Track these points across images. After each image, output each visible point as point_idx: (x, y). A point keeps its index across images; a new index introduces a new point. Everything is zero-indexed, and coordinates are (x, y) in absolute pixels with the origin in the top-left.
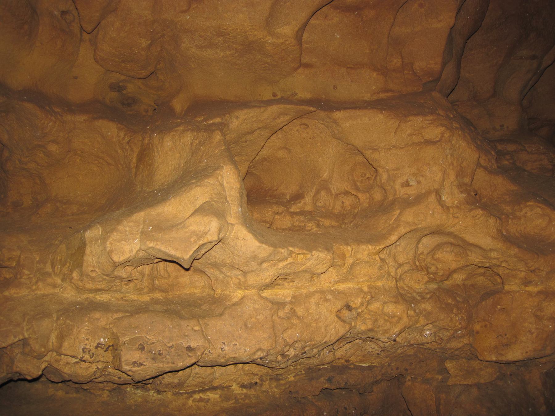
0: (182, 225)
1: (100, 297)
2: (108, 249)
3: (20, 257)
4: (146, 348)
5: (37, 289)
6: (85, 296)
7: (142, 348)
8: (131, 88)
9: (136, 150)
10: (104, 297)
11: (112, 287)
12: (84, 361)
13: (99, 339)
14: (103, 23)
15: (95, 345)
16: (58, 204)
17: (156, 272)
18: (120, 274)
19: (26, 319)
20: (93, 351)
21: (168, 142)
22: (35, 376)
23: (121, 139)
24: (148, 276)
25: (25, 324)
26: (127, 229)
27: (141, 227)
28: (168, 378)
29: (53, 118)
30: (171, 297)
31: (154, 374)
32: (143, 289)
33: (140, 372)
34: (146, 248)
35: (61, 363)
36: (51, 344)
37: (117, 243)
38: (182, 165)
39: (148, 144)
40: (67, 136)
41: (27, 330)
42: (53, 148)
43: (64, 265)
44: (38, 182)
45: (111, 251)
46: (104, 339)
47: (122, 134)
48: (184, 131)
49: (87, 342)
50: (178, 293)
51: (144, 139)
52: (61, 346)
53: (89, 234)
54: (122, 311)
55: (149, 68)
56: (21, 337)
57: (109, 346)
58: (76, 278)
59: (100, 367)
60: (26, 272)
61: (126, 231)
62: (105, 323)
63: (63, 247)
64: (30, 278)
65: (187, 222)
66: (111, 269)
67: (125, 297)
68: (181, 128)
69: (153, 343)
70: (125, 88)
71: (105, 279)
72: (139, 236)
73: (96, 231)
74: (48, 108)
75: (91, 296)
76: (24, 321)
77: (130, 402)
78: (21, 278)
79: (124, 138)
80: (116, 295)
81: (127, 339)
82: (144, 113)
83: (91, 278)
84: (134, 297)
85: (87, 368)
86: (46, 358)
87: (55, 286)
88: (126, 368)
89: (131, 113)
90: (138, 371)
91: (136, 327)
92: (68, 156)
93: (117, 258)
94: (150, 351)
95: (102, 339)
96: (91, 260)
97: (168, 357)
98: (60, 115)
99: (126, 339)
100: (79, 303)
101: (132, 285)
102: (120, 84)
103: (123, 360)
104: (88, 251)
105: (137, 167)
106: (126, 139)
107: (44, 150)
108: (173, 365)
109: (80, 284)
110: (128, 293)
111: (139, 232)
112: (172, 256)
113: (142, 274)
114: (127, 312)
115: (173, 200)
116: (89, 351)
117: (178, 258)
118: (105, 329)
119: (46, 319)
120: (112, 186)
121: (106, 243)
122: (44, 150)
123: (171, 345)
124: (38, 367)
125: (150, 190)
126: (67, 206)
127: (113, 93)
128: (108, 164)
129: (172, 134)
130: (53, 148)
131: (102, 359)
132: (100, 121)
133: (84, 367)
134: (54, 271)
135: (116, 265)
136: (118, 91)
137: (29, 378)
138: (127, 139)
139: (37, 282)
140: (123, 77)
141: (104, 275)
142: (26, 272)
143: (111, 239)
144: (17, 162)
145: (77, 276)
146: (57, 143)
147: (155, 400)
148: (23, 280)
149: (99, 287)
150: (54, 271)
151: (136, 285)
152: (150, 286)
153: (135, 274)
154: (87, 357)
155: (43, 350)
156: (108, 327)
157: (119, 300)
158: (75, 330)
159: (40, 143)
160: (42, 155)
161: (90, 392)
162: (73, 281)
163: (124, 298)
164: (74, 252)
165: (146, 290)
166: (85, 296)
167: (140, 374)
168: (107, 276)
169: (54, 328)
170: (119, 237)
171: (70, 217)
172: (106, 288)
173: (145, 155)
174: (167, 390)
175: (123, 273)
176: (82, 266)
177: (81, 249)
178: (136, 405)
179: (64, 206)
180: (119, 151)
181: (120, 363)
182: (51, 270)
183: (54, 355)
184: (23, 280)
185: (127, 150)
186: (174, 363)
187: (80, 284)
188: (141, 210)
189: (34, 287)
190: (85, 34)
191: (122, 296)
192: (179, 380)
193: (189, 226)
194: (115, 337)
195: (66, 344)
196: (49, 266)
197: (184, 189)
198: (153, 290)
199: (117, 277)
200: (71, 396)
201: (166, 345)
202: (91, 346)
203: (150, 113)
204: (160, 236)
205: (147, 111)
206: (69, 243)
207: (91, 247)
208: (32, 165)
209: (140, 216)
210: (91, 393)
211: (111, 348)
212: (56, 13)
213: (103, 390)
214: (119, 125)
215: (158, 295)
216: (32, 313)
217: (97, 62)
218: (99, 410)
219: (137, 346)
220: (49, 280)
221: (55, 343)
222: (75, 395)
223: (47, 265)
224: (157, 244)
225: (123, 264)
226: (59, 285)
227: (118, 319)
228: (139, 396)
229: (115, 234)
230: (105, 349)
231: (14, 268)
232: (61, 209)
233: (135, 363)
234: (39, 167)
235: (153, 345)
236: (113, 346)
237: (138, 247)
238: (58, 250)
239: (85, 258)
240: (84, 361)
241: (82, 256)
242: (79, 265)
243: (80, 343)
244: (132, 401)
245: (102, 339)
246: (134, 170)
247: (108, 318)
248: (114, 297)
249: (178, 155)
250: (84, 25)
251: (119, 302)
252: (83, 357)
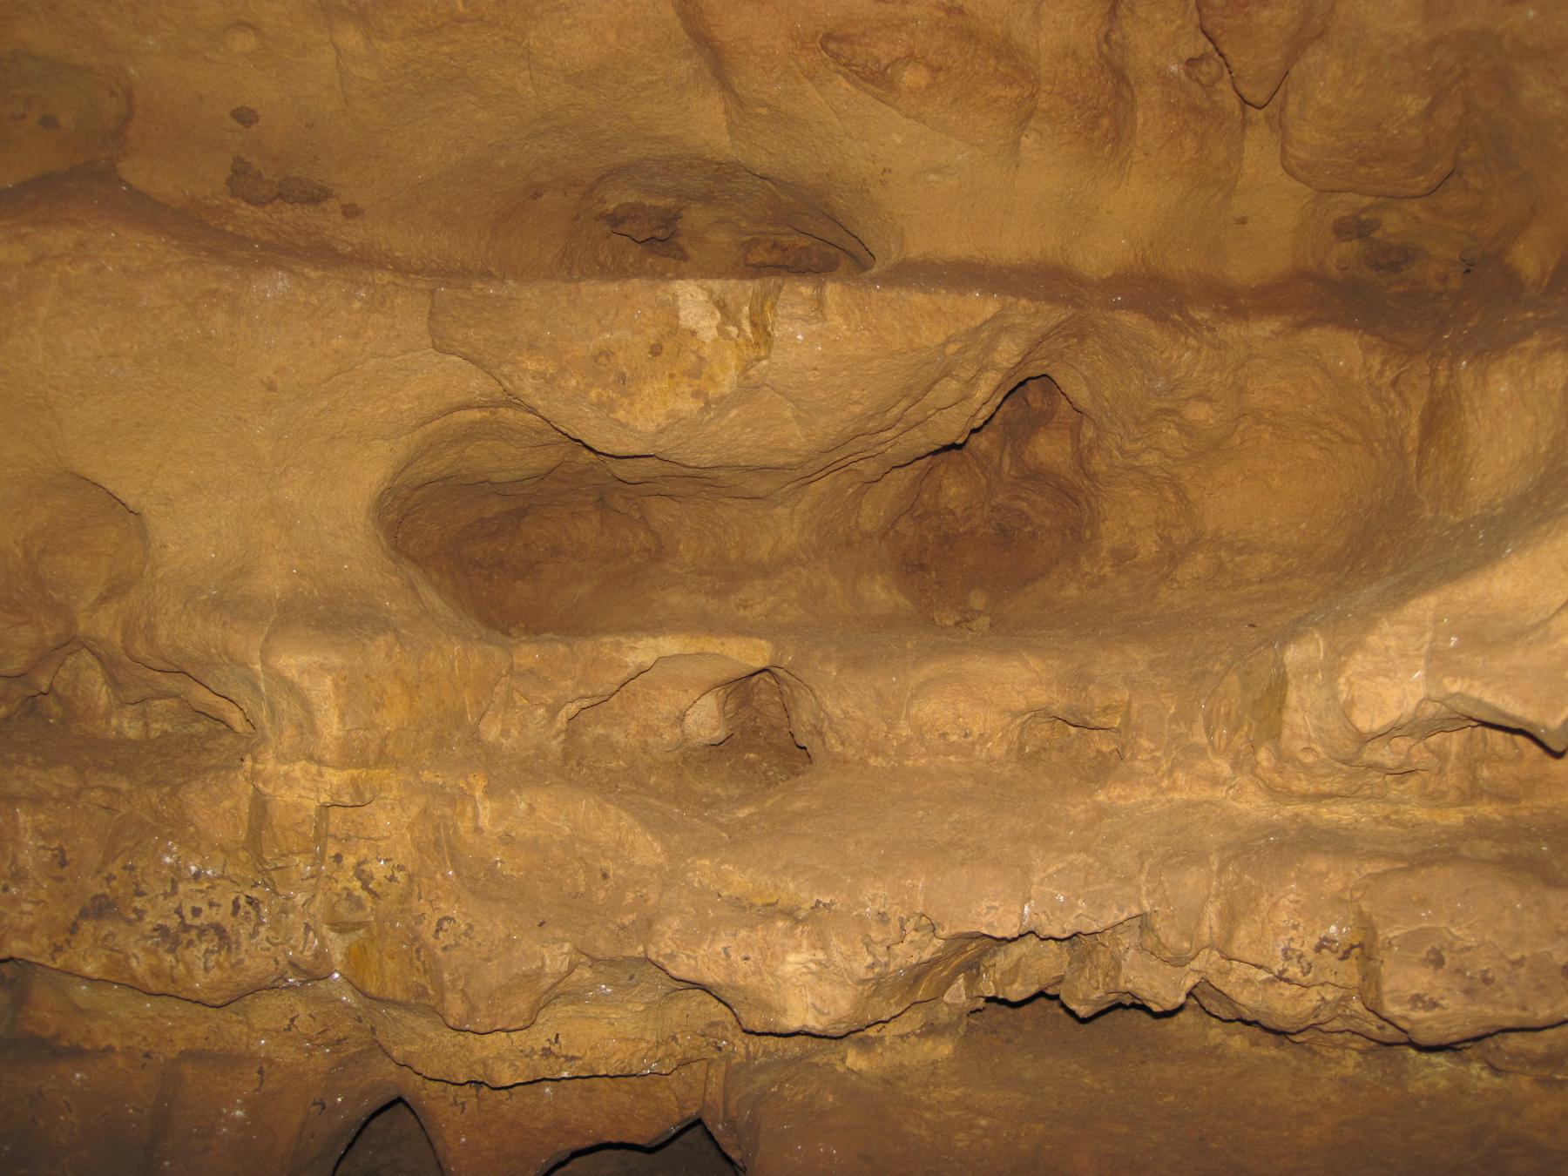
0: (1540, 632)
1: (1331, 812)
2: (1343, 697)
3: (1129, 703)
4: (1447, 960)
5: (1173, 787)
6: (1289, 810)
7: (1438, 962)
8: (1392, 224)
9: (1418, 403)
10: (1342, 814)
11: (1360, 788)
12: (1287, 980)
13: (1326, 926)
14: (1294, 72)
15: (1315, 941)
16: (1223, 554)
17: (1481, 747)
18: (1377, 758)
19: (1147, 866)
20: (1311, 956)
21: (1500, 385)
22: (1169, 1007)
23: (1374, 373)
24: (1458, 758)
25: (1143, 877)
26: (1392, 642)
27: (1428, 636)
28: (1515, 1041)
29: (1192, 342)
30: (1525, 813)
31: (1470, 1030)
32: (1444, 794)
33: (1430, 1023)
34: (1442, 695)
35: (1232, 978)
36: (1206, 930)
37: (1365, 683)
38: (1544, 449)
39: (1447, 388)
40: (1231, 379)
41: (1149, 893)
42: (1199, 413)
43: (1237, 729)
44: (1170, 496)
45: (1350, 704)
46: (1340, 929)
47: (1376, 361)
48: (1541, 352)
49: (1293, 933)
50: (1548, 803)
51: (1433, 374)
52: (1230, 937)
53: (1293, 655)
54: (1385, 855)
55: (1438, 166)
56: (1135, 911)
57: (1352, 947)
58: (1265, 763)
59: (1329, 997)
60: (1145, 743)
61: (1387, 649)
62: (1340, 885)
63: (1233, 681)
64: (1155, 759)
65: (1553, 624)
66: (1352, 748)
67: (1397, 812)
68: (1533, 343)
69: (1469, 949)
70: (1376, 224)
71: (1340, 770)
72: (1422, 662)
73: (1311, 648)
74: (1176, 316)
75: (1306, 809)
76: (1140, 871)
77: (1416, 1086)
78: (1134, 758)
79: (1381, 373)
80: (1373, 807)
81: (1397, 933)
82: (1437, 286)
83: (1304, 765)
84: (1421, 814)
85: (1295, 999)
86: (1195, 965)
87: (1215, 781)
88: (1393, 1010)
89: (1400, 289)
90: (1425, 1020)
91: (1423, 902)
92: (1241, 428)
93: (1366, 721)
94: (1458, 971)
95: (1333, 929)
96: (1301, 722)
97: (1508, 990)
98: (1211, 329)
99: (1394, 932)
100: (1278, 829)
101: (1413, 781)
102: (1364, 217)
103: (1385, 988)
104: (1292, 698)
105: (1421, 451)
106: (1388, 373)
107: (1176, 419)
108: (1524, 1014)
109: (1278, 780)
110: (1404, 803)
111: (1424, 650)
112: (1513, 718)
113: (1441, 755)
114: (1399, 857)
115: (1514, 561)
116: (1300, 957)
117: (1530, 724)
118: (1342, 901)
119: (1193, 869)
120: (1360, 501)
121: (1335, 680)
122: (1176, 419)
123: (1516, 956)
124: (1177, 985)
125: (1458, 519)
126: (1244, 557)
127: (1344, 245)
128: (1346, 440)
129: (1508, 360)
130: (1199, 413)
131: (1332, 979)
132: (1315, 331)
133: (1287, 993)
134: (1211, 743)
135: (1363, 739)
136: (1360, 236)
137: (1156, 1008)
138: (1389, 375)
139: (1171, 771)
140: (1368, 200)
141: (1337, 760)
142: (1145, 743)
143: (1349, 672)
144: (1116, 453)
145: (1268, 760)
146: (1210, 400)
147: (1485, 1090)
148: (1138, 764)
149: (1325, 788)
150: (1211, 743)
151: (1424, 785)
152: (1466, 786)
153: (1421, 756)
154: (1294, 970)
155: (1186, 945)
156: (1347, 896)
157: (1378, 823)
158: (1263, 901)
159: (1166, 405)
160: (1173, 432)
161: (1310, 1049)
162: (1259, 771)
163: (1393, 817)
164: (1258, 696)
165: (1453, 795)
166: (1289, 810)
167: (1430, 1028)
168: (1344, 763)
169: (1213, 892)
170: (1370, 667)
171: (1254, 589)
172: (1344, 792)
173: (1439, 419)
174: (1517, 1068)
175: (1386, 755)
176: (1278, 736)
177: (1275, 694)
178: (1432, 1098)
179: (1238, 559)
180: (1372, 407)
181: (1378, 997)
182: (1204, 740)
183: (1213, 959)
184: (1138, 764)
185: (1392, 405)
186: (1524, 1008)
187: (1278, 780)
188: (1427, 589)
189: (1165, 783)
190: (1251, 111)
191: (1388, 809)
192: (1550, 1047)
193: (1559, 637)
194: (1367, 926)
195: (1242, 934)
196: (1199, 726)
197: (1544, 528)
198: (1473, 796)
199: (1370, 766)
200: (1265, 1052)
201: (1502, 956)
202: (1306, 946)
203: (1455, 284)
204: (1479, 661)
205: (1444, 279)
206: (1248, 674)
207: (1299, 688)
208: (1151, 459)
209: (1425, 605)
210: (1315, 1053)
211: (1356, 951)
212: (1174, 68)
213: (1344, 1047)
214: (1366, 338)
215: (1487, 810)
216: (1161, 850)
217: (1292, 174)
218: (1333, 1098)
219: (1423, 954)
220: (1202, 766)
221: (1216, 929)
222: (1273, 1052)
223: (1195, 726)
224: (1471, 686)
225: (1387, 734)
226: (1226, 779)
227: (1375, 877)
228: (1442, 1074)
229: (1359, 657)
230: (1340, 954)
231: (1118, 731)
232: (1230, 566)
233: (1416, 999)
234: (1170, 461)
235: (1467, 954)
236: (1361, 945)
237: (1421, 692)
238: (1221, 690)
239: (1286, 717)
240: (1287, 980)
241: (1280, 711)
242: (1271, 731)
243: (1276, 935)
244: (1420, 1084)
245: (1333, 929)
246: (1414, 459)
247: (1349, 874)
248: (1369, 813)
249: (1529, 419)
250: (1246, 91)
251: (1381, 828)
252: (1285, 970)
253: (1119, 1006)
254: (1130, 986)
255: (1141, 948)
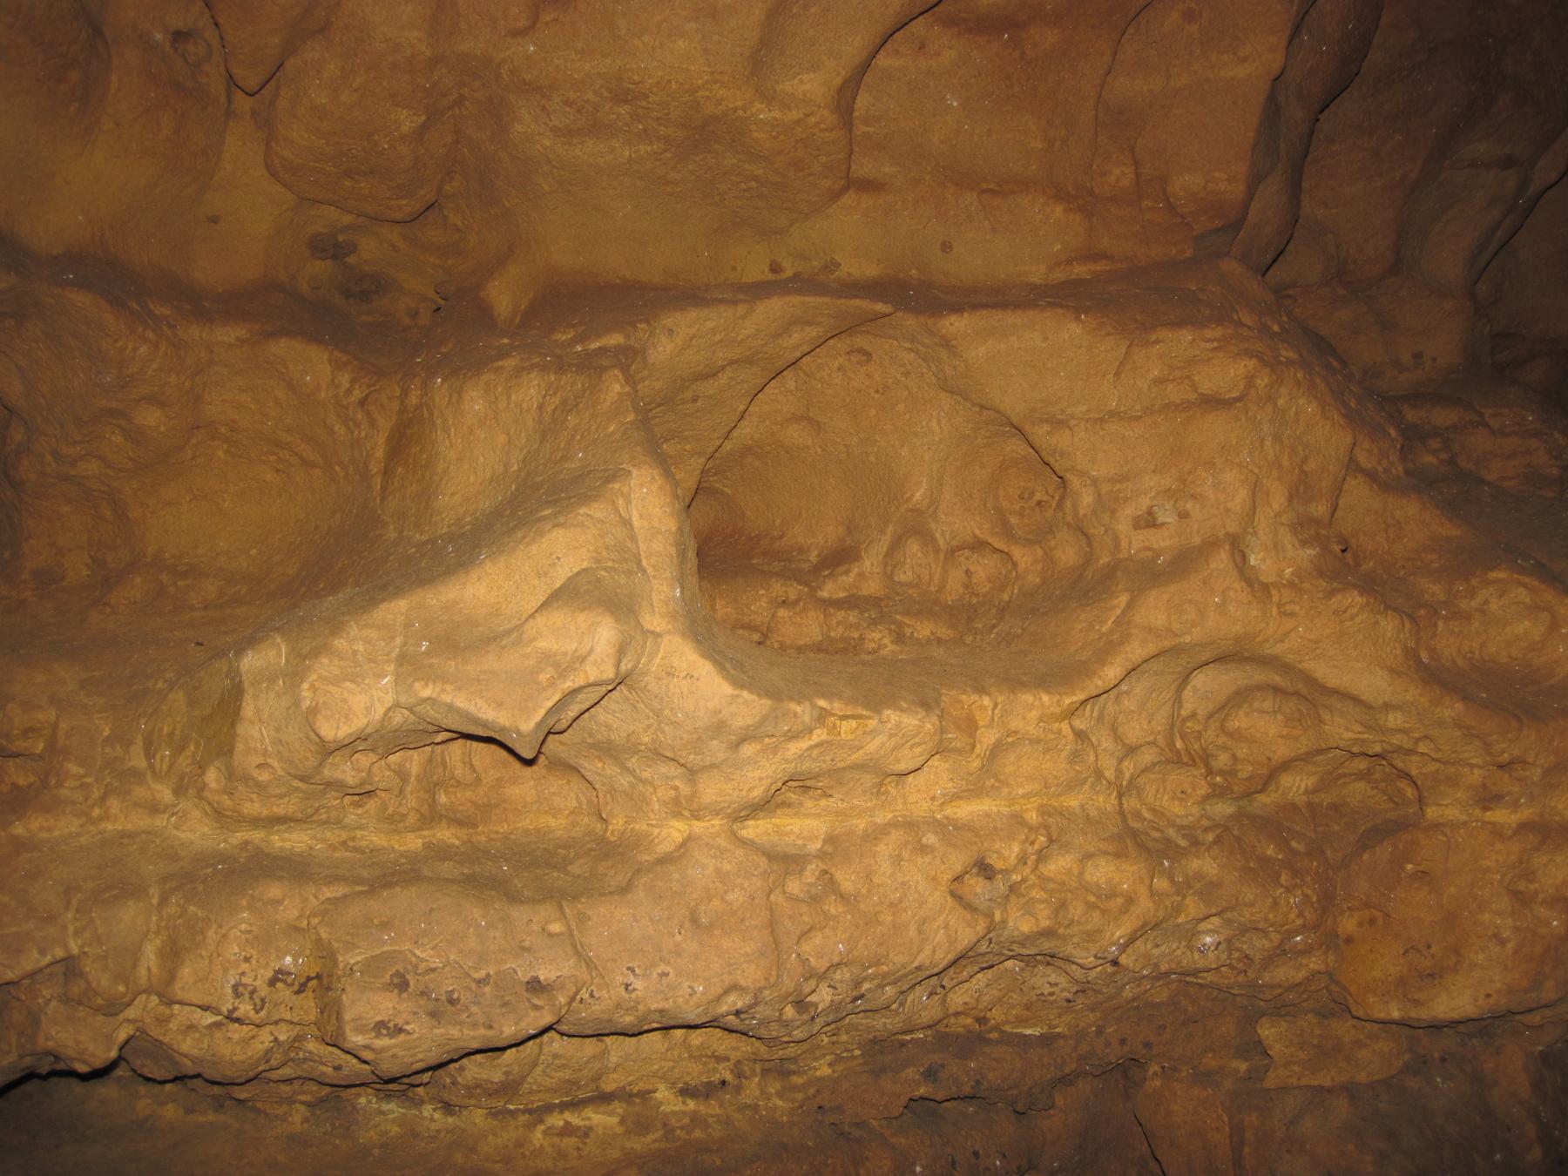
0: (514, 635)
1: (283, 840)
2: (306, 704)
3: (56, 726)
4: (412, 983)
5: (105, 817)
6: (239, 837)
7: (401, 985)
8: (369, 249)
9: (386, 424)
10: (295, 841)
11: (317, 810)
12: (238, 1020)
13: (280, 958)
15: (270, 974)
16: (164, 577)
17: (441, 770)
18: (338, 775)
19: (74, 902)
20: (264, 991)
21: (475, 402)
22: (98, 1063)
23: (341, 392)
24: (418, 779)
25: (70, 915)
26: (360, 647)
27: (399, 640)
28: (474, 1070)
29: (150, 335)
30: (483, 838)
31: (434, 1057)
32: (404, 817)
33: (395, 1051)
34: (412, 700)
35: (173, 1025)
36: (143, 972)
37: (330, 688)
39: (419, 407)
40: (188, 384)
41: (77, 933)
42: (150, 418)
43: (182, 749)
44: (108, 514)
45: (314, 711)
46: (295, 959)
47: (345, 379)
49: (245, 966)
50: (503, 828)
51: (406, 392)
52: (172, 977)
53: (251, 662)
54: (345, 879)
56: (60, 953)
57: (309, 979)
58: (213, 785)
59: (282, 1038)
60: (74, 769)
61: (355, 653)
62: (296, 913)
63: (178, 697)
64: (84, 786)
65: (527, 626)
66: (313, 761)
67: (354, 839)
69: (434, 970)
70: (352, 248)
71: (297, 789)
72: (391, 668)
73: (272, 653)
74: (135, 306)
75: (257, 836)
76: (67, 908)
77: (367, 1136)
78: (60, 785)
79: (349, 391)
80: (328, 834)
81: (359, 958)
82: (407, 321)
83: (258, 785)
84: (378, 840)
85: (246, 1042)
86: (131, 1013)
87: (154, 808)
88: (356, 1039)
89: (371, 319)
90: (390, 1048)
91: (386, 925)
92: (194, 441)
93: (330, 730)
94: (423, 993)
95: (289, 959)
96: (256, 734)
97: (475, 1009)
98: (171, 326)
99: (355, 958)
100: (223, 857)
101: (372, 805)
102: (340, 238)
103: (347, 1017)
104: (248, 709)
105: (387, 472)
106: (357, 392)
107: (123, 423)
108: (490, 1033)
109: (227, 801)
110: (361, 828)
111: (393, 655)
112: (485, 724)
113: (402, 775)
114: (359, 881)
115: (488, 566)
116: (253, 992)
117: (503, 729)
118: (297, 929)
119: (131, 903)
120: (317, 527)
121: (299, 686)
122: (123, 423)
123: (482, 974)
124: (109, 1038)
125: (424, 538)
126: (189, 581)
127: (318, 263)
128: (306, 463)
129: (485, 377)
130: (150, 418)
131: (288, 1016)
132: (283, 342)
133: (236, 1037)
134: (151, 766)
135: (328, 750)
136: (334, 257)
137: (82, 1068)
138: (358, 394)
139: (103, 799)
140: (348, 219)
141: (295, 777)
142: (74, 769)
143: (314, 677)
144: (49, 458)
145: (217, 781)
146: (162, 405)
147: (438, 1131)
148: (64, 792)
149: (279, 810)
150: (151, 766)
151: (384, 807)
152: (425, 809)
153: (383, 775)
154: (245, 1009)
155: (122, 988)
156: (304, 924)
157: (335, 849)
158: (211, 933)
159: (113, 405)
160: (118, 438)
161: (253, 1109)
162: (205, 793)
163: (351, 844)
164: (208, 712)
165: (412, 819)
166: (239, 837)
167: (394, 1056)
168: (303, 779)
169: (153, 927)
170: (336, 671)
171: (197, 614)
172: (300, 815)
173: (408, 439)
174: (473, 1102)
175: (346, 771)
176: (231, 751)
177: (230, 704)
178: (384, 1146)
179: (180, 583)
180: (337, 427)
181: (340, 1027)
182: (144, 764)
183: (152, 1005)
184: (64, 792)
185: (358, 425)
186: (491, 1027)
187: (227, 801)
188: (398, 592)
189: (96, 812)
190: (239, 97)
191: (344, 835)
192: (507, 1073)
193: (534, 639)
194: (326, 954)
195: (186, 972)
196: (137, 751)
197: (519, 534)
198: (432, 819)
199: (330, 784)
200: (202, 1119)
201: (468, 975)
202: (258, 978)
203: (424, 320)
204: (451, 666)
205: (415, 315)
206: (196, 688)
207: (256, 697)
208: (91, 468)
209: (396, 610)
210: (258, 1112)
211: (313, 983)
213: (291, 1101)
214: (337, 354)
215: (446, 835)
216: (91, 885)
217: (274, 175)
218: (280, 1158)
219: (387, 978)
220: (140, 792)
221: (155, 971)
222: (211, 1117)
223: (132, 748)
224: (443, 690)
225: (348, 747)
226: (167, 807)
227: (333, 901)
228: (393, 1121)
229: (325, 661)
230: (296, 987)
231: (41, 757)
232: (172, 590)
233: (380, 1025)
234: (111, 473)
235: (432, 975)
236: (318, 977)
237: (389, 699)
238: (164, 707)
239: (241, 729)
240: (238, 1020)
241: (233, 725)
242: (223, 748)
243: (226, 970)
244: (372, 1133)
245: (289, 959)
246: (378, 480)
247: (306, 900)
248: (323, 840)
249: (503, 438)
251: (337, 855)
252: (235, 1009)
253: (30, 1076)
254: (51, 1044)
255: (66, 999)
